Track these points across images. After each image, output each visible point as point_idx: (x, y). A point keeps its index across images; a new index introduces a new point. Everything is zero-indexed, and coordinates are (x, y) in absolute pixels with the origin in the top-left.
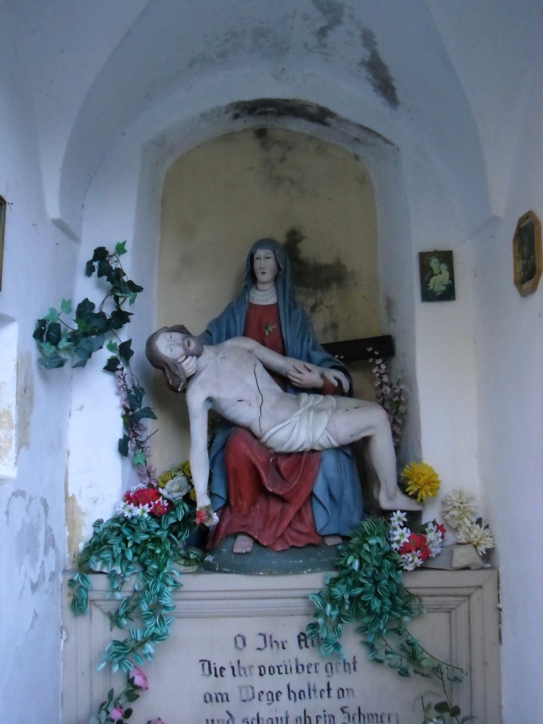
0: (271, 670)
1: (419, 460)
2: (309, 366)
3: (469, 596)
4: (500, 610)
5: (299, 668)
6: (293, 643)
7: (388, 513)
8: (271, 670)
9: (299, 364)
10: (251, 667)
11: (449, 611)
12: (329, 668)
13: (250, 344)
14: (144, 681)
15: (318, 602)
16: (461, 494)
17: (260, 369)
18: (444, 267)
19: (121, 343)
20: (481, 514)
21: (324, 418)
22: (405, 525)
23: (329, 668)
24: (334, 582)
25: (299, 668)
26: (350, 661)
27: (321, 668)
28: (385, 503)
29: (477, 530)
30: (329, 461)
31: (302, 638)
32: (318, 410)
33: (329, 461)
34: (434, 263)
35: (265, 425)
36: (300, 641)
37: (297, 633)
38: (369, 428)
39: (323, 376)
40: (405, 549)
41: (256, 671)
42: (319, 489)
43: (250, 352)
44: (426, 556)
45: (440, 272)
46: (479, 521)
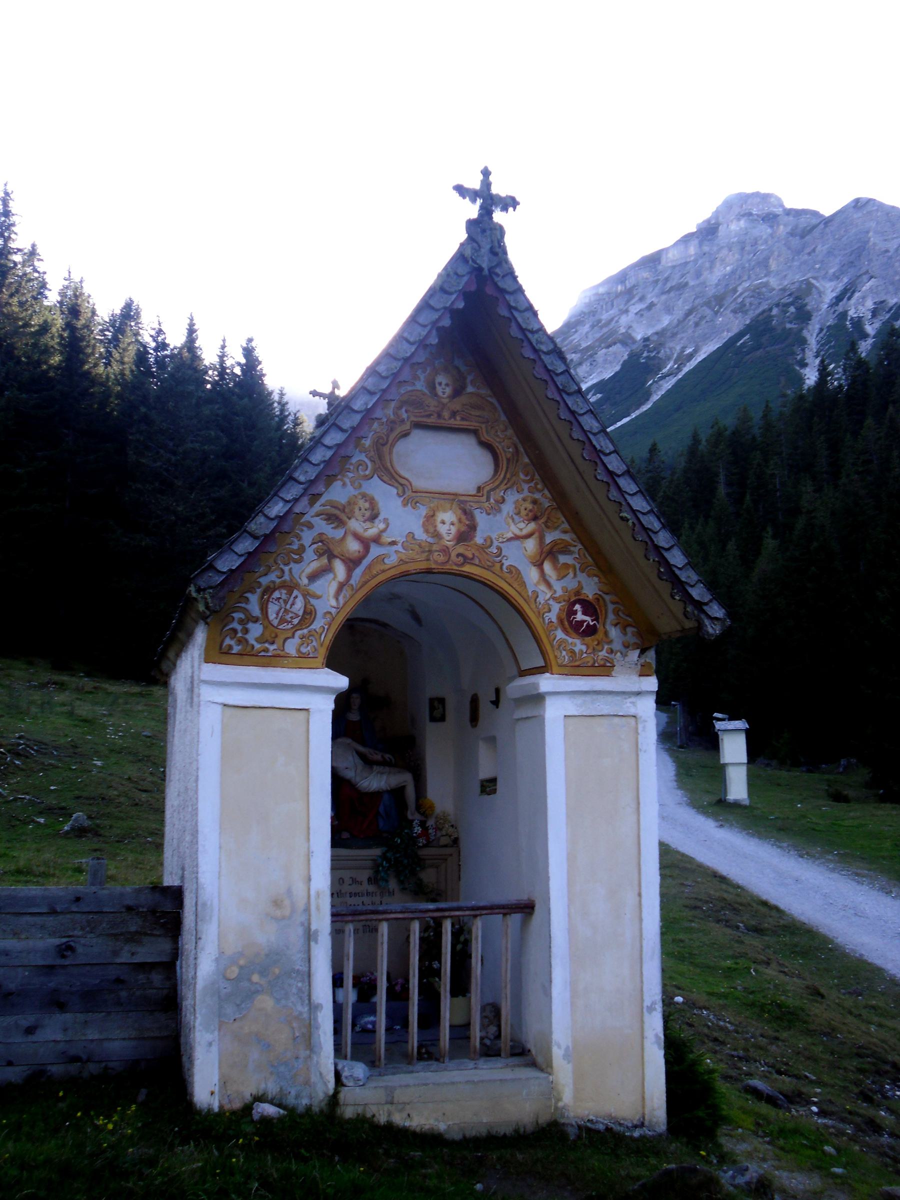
0: (356, 894)
1: (426, 797)
2: (376, 752)
3: (446, 860)
4: (460, 865)
5: (368, 894)
6: (365, 882)
7: (413, 821)
8: (356, 894)
9: (371, 751)
10: (346, 893)
11: (437, 867)
12: (382, 895)
13: (349, 741)
14: (539, 580)
15: (379, 861)
16: (444, 813)
17: (354, 753)
18: (440, 706)
19: (654, 697)
20: (453, 823)
21: (385, 777)
22: (419, 826)
23: (382, 895)
24: (387, 852)
25: (368, 894)
26: (391, 890)
27: (378, 893)
28: (410, 817)
29: (451, 830)
30: (386, 797)
31: (369, 880)
32: (382, 773)
33: (386, 797)
34: (436, 704)
35: (358, 779)
36: (368, 881)
37: (367, 877)
38: (405, 781)
39: (382, 756)
40: (419, 836)
41: (348, 895)
42: (381, 809)
43: (349, 744)
44: (428, 839)
45: (759, 264)
46: (452, 826)
